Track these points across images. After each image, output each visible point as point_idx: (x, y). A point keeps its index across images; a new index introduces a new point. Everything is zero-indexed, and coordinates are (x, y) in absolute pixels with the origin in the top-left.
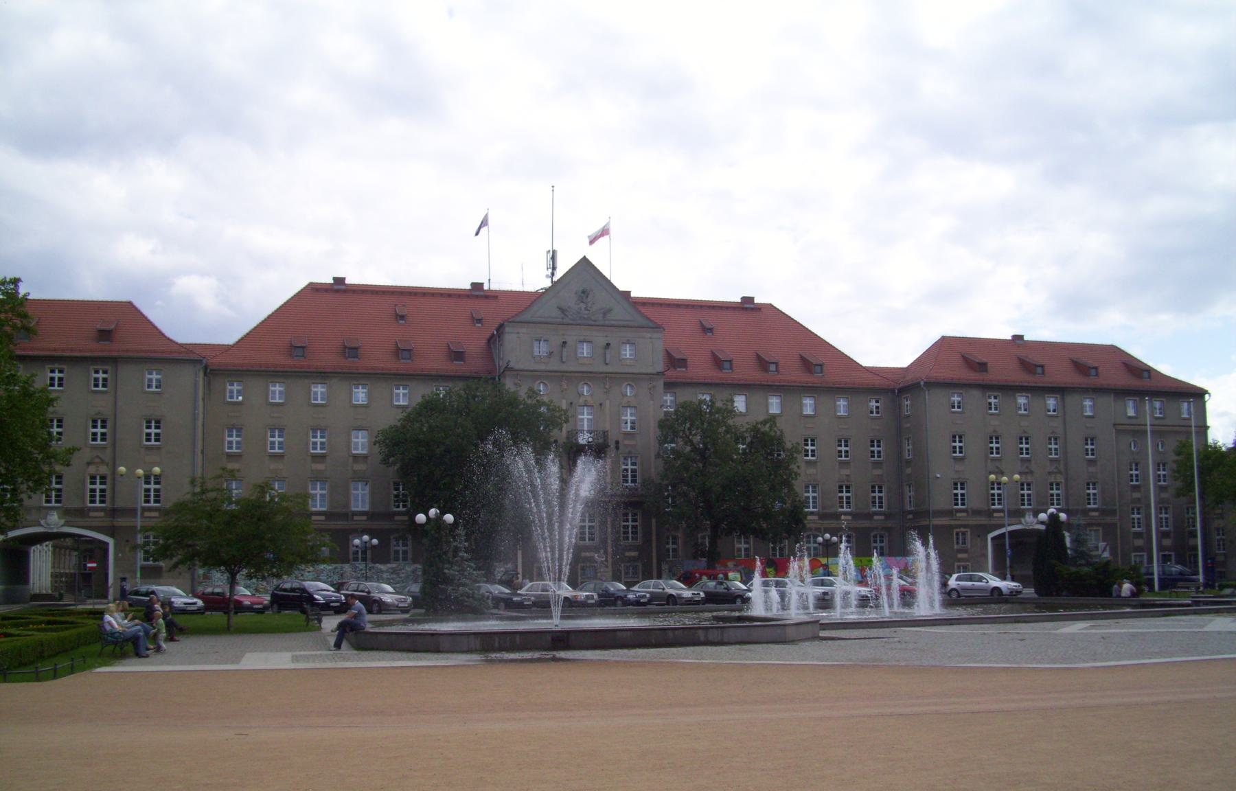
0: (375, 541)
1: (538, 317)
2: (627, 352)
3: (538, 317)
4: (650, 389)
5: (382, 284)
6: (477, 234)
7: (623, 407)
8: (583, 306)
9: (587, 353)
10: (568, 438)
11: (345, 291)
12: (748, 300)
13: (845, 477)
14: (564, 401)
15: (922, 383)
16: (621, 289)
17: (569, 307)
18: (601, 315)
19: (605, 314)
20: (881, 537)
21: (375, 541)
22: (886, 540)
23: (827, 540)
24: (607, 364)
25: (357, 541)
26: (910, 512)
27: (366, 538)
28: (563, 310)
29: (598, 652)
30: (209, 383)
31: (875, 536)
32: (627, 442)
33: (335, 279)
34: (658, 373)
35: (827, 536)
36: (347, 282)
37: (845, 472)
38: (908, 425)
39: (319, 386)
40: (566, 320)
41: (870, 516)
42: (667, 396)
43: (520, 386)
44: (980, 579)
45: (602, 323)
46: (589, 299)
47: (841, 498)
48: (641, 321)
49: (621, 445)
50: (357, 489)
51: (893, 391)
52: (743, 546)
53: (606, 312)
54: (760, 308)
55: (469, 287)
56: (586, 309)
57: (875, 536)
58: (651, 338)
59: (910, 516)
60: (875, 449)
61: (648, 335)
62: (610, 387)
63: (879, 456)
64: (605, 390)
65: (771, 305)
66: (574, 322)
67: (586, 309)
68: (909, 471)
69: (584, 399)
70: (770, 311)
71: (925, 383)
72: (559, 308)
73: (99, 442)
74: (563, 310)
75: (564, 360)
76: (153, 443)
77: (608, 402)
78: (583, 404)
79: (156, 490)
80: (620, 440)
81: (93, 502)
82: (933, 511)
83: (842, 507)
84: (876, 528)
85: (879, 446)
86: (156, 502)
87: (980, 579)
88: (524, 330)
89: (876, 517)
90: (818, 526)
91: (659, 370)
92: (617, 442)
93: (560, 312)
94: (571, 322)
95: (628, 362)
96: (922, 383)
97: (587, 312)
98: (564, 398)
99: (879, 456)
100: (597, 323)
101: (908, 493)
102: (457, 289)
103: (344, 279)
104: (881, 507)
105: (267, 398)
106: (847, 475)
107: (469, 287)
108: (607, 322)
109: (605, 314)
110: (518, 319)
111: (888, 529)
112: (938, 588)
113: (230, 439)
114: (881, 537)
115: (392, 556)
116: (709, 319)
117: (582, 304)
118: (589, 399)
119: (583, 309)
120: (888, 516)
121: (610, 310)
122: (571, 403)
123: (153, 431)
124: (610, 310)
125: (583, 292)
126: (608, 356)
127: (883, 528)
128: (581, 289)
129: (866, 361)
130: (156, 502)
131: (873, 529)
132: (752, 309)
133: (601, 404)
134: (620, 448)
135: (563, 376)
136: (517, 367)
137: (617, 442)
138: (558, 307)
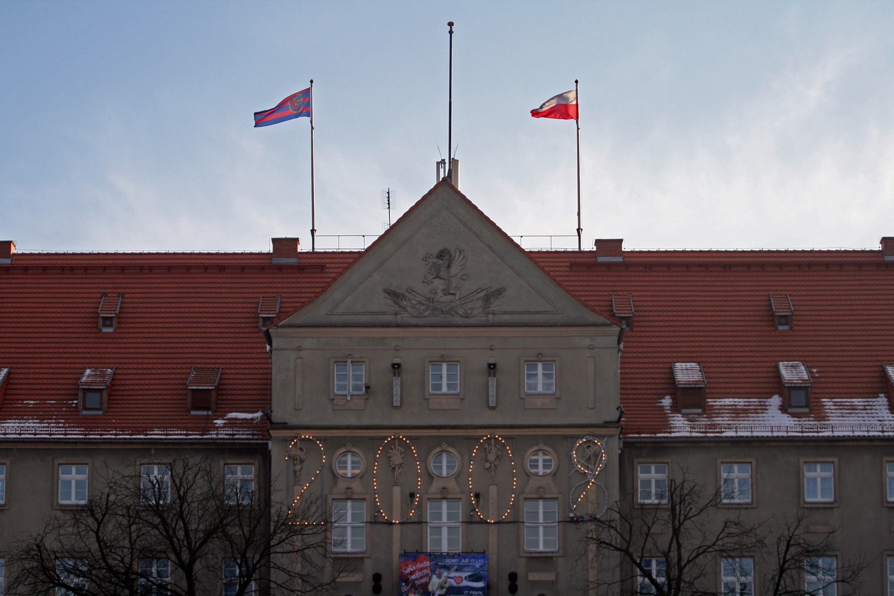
1: (343, 314)
3: (343, 314)
5: (731, 248)
7: (526, 499)
11: (300, 268)
16: (527, 245)
17: (411, 290)
18: (479, 304)
19: (487, 299)
24: (493, 408)
32: (534, 576)
33: (598, 242)
34: (606, 422)
36: (626, 247)
39: (819, 467)
40: (405, 318)
42: (815, 471)
43: (302, 461)
46: (454, 270)
49: (520, 582)
53: (491, 296)
55: (877, 246)
56: (447, 292)
58: (590, 348)
64: (488, 465)
66: (421, 321)
67: (447, 292)
69: (442, 485)
75: (492, 403)
77: (493, 490)
78: (439, 496)
80: (520, 571)
91: (608, 418)
92: (513, 577)
93: (390, 302)
94: (414, 321)
95: (539, 402)
97: (449, 298)
98: (396, 484)
100: (472, 321)
102: (812, 252)
103: (621, 241)
107: (877, 246)
109: (487, 299)
117: (437, 282)
118: (452, 485)
119: (440, 294)
125: (440, 256)
128: (435, 251)
134: (519, 588)
137: (513, 577)
138: (385, 291)
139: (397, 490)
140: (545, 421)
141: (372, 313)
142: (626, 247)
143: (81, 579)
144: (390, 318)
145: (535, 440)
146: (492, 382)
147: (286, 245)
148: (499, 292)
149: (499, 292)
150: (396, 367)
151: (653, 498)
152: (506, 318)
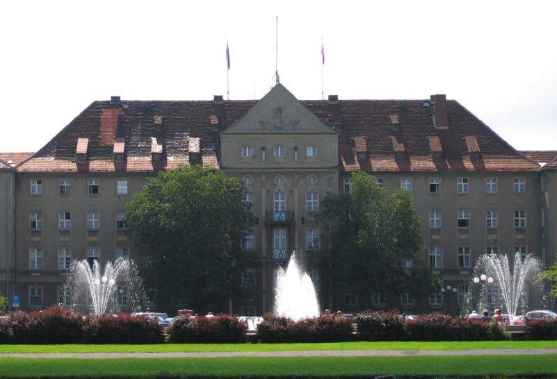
2: (310, 152)
4: (328, 180)
9: (39, 191)
10: (267, 218)
14: (264, 190)
23: (449, 291)
29: (227, 346)
35: (449, 287)
36: (339, 98)
45: (292, 132)
50: (433, 217)
56: (280, 122)
62: (298, 179)
67: (280, 122)
77: (296, 190)
92: (303, 219)
94: (269, 132)
97: (281, 124)
100: (289, 132)
108: (295, 132)
112: (333, 355)
113: (277, 201)
122: (269, 191)
125: (278, 110)
133: (291, 191)
135: (295, 172)
137: (303, 219)
139: (264, 190)
140: (314, 166)
141: (262, 169)
142: (339, 98)
143: (217, 246)
144: (261, 131)
145: (311, 173)
146: (296, 153)
147: (218, 98)
148: (298, 122)
149: (298, 122)
150: (263, 149)
151: (264, 263)
152: (300, 131)
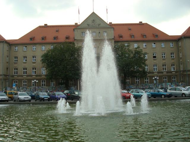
0: (37, 81)
6: (79, 14)
8: (93, 24)
12: (141, 22)
13: (164, 63)
15: (183, 37)
20: (175, 77)
21: (37, 81)
22: (176, 78)
25: (33, 81)
26: (182, 71)
27: (35, 80)
28: (88, 25)
30: (11, 47)
31: (164, 78)
37: (164, 61)
38: (180, 49)
41: (162, 73)
44: (179, 90)
45: (98, 27)
47: (163, 68)
48: (110, 27)
51: (176, 40)
52: (128, 81)
53: (99, 25)
54: (143, 24)
55: (74, 24)
57: (164, 78)
59: (182, 72)
60: (172, 55)
61: (110, 29)
63: (173, 57)
65: (146, 23)
68: (181, 60)
70: (146, 24)
71: (184, 37)
72: (87, 24)
73: (16, 62)
74: (88, 25)
76: (16, 62)
79: (26, 71)
81: (24, 74)
82: (187, 70)
83: (155, 71)
84: (173, 75)
85: (173, 55)
86: (26, 74)
87: (179, 90)
88: (78, 30)
89: (173, 73)
90: (157, 75)
96: (183, 37)
99: (173, 57)
101: (181, 66)
104: (165, 70)
105: (23, 50)
106: (165, 62)
110: (77, 28)
111: (176, 76)
114: (175, 77)
115: (32, 85)
116: (131, 27)
120: (176, 72)
121: (100, 24)
123: (16, 59)
124: (100, 24)
125: (93, 20)
126: (100, 35)
127: (175, 75)
129: (170, 35)
130: (17, 74)
131: (163, 76)
132: (142, 24)
136: (77, 39)
